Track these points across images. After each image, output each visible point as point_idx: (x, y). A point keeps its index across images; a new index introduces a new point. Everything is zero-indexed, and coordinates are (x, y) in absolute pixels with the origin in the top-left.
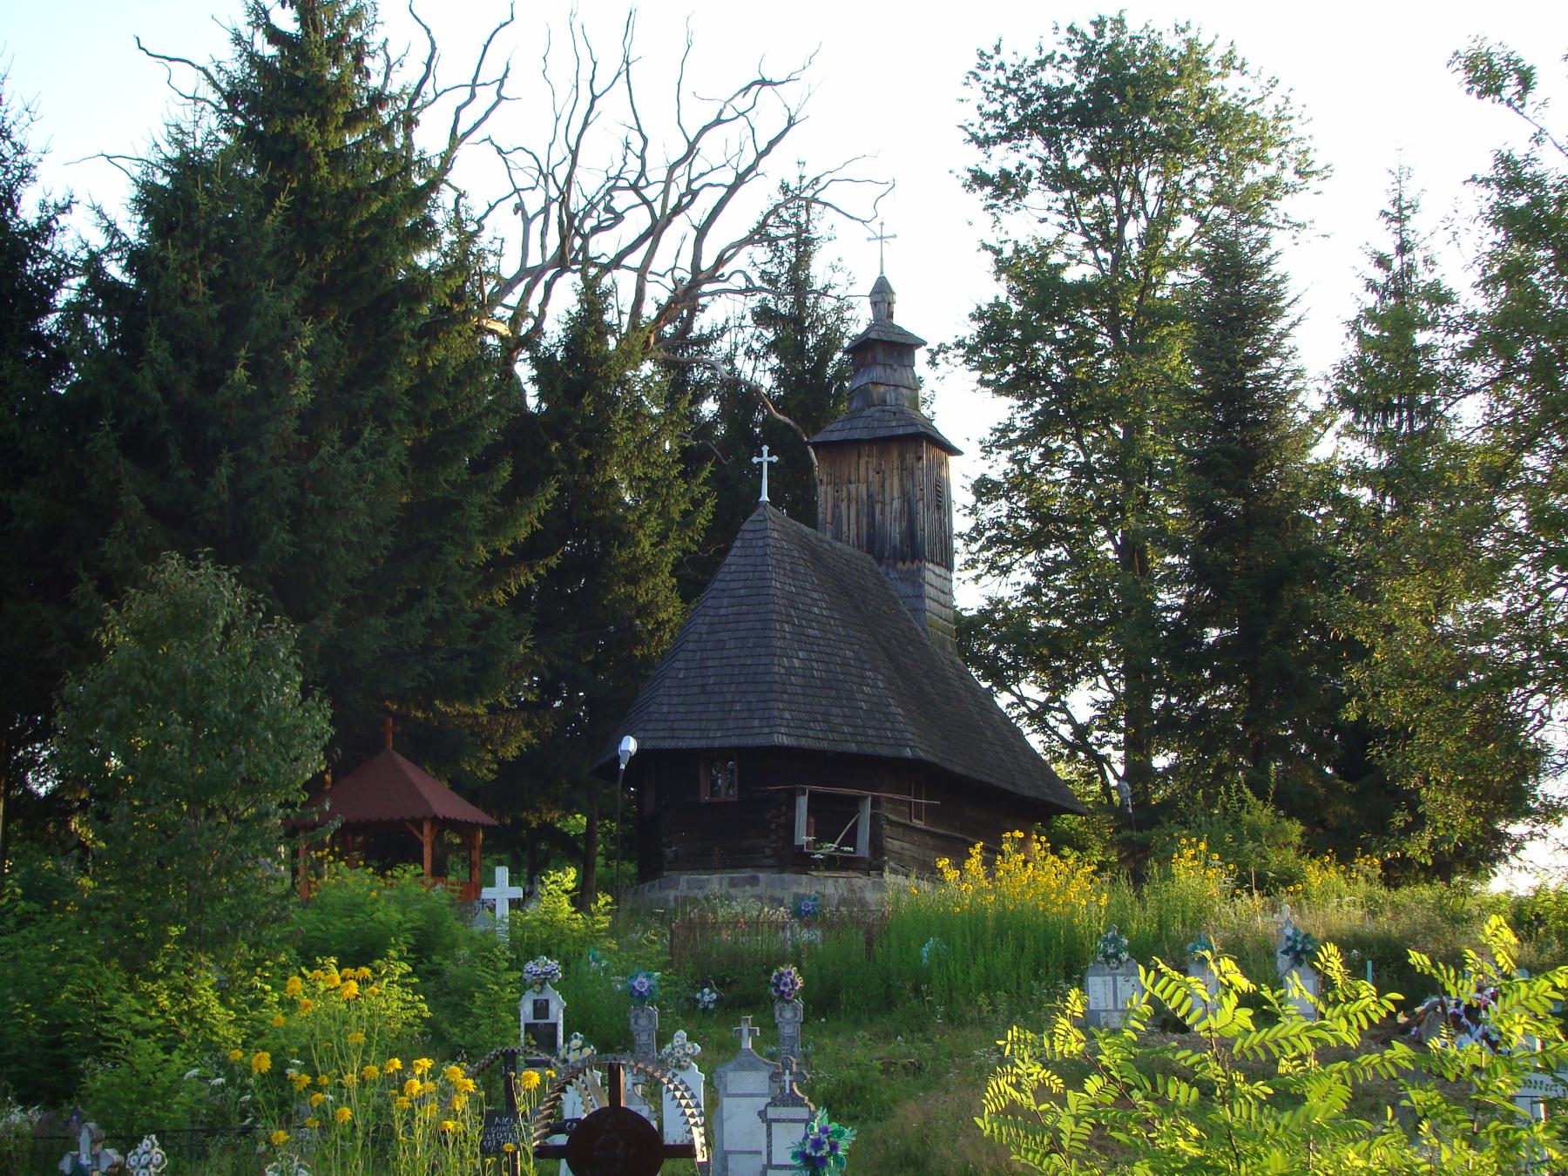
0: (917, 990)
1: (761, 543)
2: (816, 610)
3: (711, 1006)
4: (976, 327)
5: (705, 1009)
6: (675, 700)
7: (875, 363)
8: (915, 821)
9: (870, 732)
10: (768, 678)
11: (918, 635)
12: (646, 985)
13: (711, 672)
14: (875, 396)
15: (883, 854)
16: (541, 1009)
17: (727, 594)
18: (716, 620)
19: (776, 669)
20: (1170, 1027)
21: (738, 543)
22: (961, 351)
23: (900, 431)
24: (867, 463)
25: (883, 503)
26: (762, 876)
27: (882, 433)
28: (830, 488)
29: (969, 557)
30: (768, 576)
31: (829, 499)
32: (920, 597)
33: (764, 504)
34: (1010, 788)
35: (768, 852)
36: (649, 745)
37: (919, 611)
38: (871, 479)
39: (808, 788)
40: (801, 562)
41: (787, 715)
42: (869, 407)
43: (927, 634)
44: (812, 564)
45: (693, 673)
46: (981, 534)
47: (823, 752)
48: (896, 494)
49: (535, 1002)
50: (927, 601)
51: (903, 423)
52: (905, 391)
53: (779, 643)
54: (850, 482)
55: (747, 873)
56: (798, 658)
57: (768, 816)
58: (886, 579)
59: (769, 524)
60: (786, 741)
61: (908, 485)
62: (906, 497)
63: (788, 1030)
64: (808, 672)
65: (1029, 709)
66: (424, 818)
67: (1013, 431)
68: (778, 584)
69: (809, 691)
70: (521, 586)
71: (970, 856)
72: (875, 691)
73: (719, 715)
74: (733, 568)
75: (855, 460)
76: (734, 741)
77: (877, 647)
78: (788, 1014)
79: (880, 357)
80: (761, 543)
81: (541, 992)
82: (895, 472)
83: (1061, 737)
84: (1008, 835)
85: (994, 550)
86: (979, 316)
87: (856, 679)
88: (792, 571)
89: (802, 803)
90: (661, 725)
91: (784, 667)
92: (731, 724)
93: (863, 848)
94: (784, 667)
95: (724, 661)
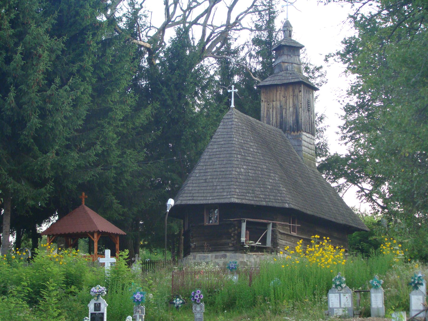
0: (265, 300)
1: (230, 123)
2: (252, 150)
3: (180, 306)
4: (344, 46)
5: (177, 307)
6: (194, 185)
7: (284, 54)
8: (292, 233)
9: (271, 197)
10: (231, 176)
11: (299, 160)
12: (140, 297)
13: (209, 174)
14: (283, 67)
15: (277, 246)
16: (97, 307)
17: (216, 143)
18: (212, 153)
19: (234, 173)
20: (362, 314)
21: (221, 124)
22: (339, 56)
23: (293, 81)
24: (280, 93)
25: (286, 109)
26: (228, 254)
27: (286, 81)
28: (266, 104)
29: (343, 135)
30: (232, 136)
31: (265, 107)
32: (300, 145)
33: (233, 108)
34: (333, 220)
35: (230, 245)
36: (179, 202)
37: (300, 151)
38: (281, 100)
39: (246, 219)
40: (246, 131)
41: (237, 191)
42: (281, 72)
43: (303, 160)
44: (252, 132)
45: (202, 174)
46: (347, 126)
47: (252, 206)
48: (291, 106)
49: (95, 304)
50: (303, 147)
51: (294, 78)
52: (295, 65)
53: (236, 163)
54: (273, 101)
55: (223, 253)
56: (243, 168)
57: (230, 231)
58: (287, 138)
59: (234, 116)
60: (237, 201)
61: (296, 102)
62: (295, 107)
63: (198, 316)
64: (247, 174)
65: (365, 193)
66: (94, 232)
67: (360, 87)
68: (236, 140)
69: (247, 181)
70: (146, 143)
71: (297, 245)
72: (274, 181)
73: (211, 191)
74: (219, 133)
75: (275, 92)
76: (217, 201)
77: (277, 164)
78: (198, 309)
79: (286, 51)
80: (230, 123)
81: (97, 300)
82: (291, 97)
83: (378, 204)
84: (313, 237)
85: (353, 132)
86: (345, 42)
87: (266, 177)
88: (243, 134)
89: (244, 226)
90: (189, 195)
91: (237, 172)
92: (215, 194)
93: (269, 243)
94: (237, 172)
95: (214, 170)
